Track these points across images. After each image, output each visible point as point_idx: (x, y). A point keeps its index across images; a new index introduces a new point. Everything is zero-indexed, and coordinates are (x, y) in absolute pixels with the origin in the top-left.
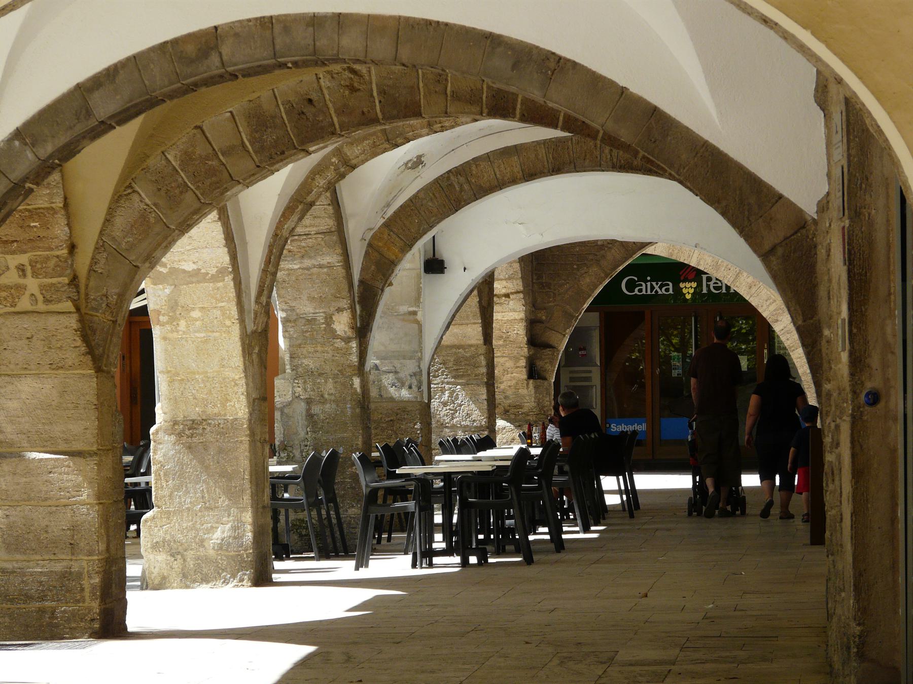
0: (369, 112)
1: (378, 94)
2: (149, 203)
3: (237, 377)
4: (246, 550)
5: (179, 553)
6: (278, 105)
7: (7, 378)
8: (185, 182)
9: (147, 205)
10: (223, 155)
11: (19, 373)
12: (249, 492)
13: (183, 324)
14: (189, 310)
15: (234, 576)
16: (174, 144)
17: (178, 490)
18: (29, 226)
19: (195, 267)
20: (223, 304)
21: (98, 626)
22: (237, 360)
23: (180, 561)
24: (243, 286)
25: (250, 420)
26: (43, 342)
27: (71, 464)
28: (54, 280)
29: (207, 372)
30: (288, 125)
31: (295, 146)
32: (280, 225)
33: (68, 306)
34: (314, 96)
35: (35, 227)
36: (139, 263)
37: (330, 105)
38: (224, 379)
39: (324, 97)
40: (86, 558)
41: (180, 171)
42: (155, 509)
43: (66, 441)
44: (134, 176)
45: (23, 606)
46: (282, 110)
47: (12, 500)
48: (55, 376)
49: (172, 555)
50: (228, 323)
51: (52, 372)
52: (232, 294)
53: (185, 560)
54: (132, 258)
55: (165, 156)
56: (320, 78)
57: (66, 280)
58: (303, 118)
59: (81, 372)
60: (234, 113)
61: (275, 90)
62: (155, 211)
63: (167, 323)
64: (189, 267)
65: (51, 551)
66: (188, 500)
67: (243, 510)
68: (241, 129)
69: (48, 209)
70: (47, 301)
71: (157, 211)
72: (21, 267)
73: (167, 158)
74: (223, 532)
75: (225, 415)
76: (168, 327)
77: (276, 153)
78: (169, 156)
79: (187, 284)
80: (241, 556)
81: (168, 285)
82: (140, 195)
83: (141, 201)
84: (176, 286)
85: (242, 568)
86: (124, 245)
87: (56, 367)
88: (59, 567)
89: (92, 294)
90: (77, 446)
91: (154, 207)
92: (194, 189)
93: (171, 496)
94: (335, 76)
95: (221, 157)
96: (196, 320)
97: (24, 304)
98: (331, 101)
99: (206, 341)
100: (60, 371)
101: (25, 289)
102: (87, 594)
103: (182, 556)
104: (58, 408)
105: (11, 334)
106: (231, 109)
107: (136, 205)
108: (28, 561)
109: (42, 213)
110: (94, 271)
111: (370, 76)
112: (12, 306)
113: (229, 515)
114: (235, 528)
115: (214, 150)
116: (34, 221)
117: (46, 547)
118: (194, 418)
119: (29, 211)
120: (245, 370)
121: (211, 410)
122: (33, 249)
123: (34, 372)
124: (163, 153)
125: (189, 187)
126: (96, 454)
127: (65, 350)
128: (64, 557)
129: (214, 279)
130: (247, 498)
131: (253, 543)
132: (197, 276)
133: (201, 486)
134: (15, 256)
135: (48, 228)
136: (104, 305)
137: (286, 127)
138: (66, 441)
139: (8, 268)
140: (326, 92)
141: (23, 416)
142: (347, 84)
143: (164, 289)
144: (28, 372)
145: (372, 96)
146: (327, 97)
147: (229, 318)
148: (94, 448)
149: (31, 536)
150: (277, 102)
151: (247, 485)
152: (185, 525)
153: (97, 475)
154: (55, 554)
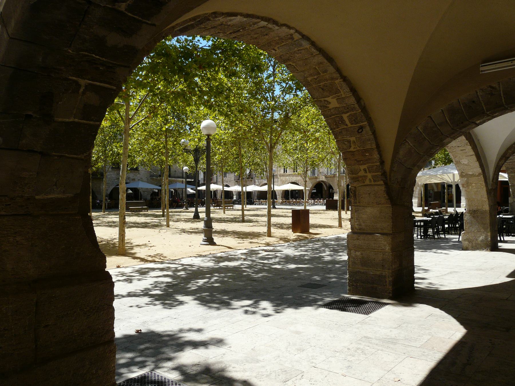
2: (412, 145)
7: (363, 207)
8: (425, 137)
9: (411, 146)
10: (439, 126)
12: (489, 228)
13: (470, 187)
15: (486, 249)
25: (490, 211)
27: (383, 238)
28: (376, 174)
32: (498, 163)
35: (368, 155)
40: (387, 271)
49: (469, 242)
50: (482, 187)
52: (483, 179)
57: (380, 174)
59: (387, 205)
61: (459, 99)
64: (471, 173)
67: (488, 232)
68: (446, 115)
69: (371, 148)
70: (375, 181)
73: (418, 129)
74: (482, 237)
76: (467, 188)
78: (419, 128)
82: (409, 143)
85: (488, 247)
87: (378, 204)
88: (378, 273)
90: (385, 231)
93: (469, 228)
94: (484, 90)
97: (367, 182)
98: (482, 101)
99: (477, 191)
106: (442, 109)
111: (499, 87)
112: (363, 183)
113: (484, 234)
114: (486, 237)
115: (435, 124)
118: (475, 209)
120: (488, 198)
123: (371, 205)
124: (417, 127)
126: (391, 234)
129: (478, 176)
130: (489, 230)
132: (473, 175)
134: (362, 166)
139: (361, 170)
140: (480, 97)
144: (369, 205)
146: (481, 99)
148: (391, 232)
150: (460, 103)
151: (489, 226)
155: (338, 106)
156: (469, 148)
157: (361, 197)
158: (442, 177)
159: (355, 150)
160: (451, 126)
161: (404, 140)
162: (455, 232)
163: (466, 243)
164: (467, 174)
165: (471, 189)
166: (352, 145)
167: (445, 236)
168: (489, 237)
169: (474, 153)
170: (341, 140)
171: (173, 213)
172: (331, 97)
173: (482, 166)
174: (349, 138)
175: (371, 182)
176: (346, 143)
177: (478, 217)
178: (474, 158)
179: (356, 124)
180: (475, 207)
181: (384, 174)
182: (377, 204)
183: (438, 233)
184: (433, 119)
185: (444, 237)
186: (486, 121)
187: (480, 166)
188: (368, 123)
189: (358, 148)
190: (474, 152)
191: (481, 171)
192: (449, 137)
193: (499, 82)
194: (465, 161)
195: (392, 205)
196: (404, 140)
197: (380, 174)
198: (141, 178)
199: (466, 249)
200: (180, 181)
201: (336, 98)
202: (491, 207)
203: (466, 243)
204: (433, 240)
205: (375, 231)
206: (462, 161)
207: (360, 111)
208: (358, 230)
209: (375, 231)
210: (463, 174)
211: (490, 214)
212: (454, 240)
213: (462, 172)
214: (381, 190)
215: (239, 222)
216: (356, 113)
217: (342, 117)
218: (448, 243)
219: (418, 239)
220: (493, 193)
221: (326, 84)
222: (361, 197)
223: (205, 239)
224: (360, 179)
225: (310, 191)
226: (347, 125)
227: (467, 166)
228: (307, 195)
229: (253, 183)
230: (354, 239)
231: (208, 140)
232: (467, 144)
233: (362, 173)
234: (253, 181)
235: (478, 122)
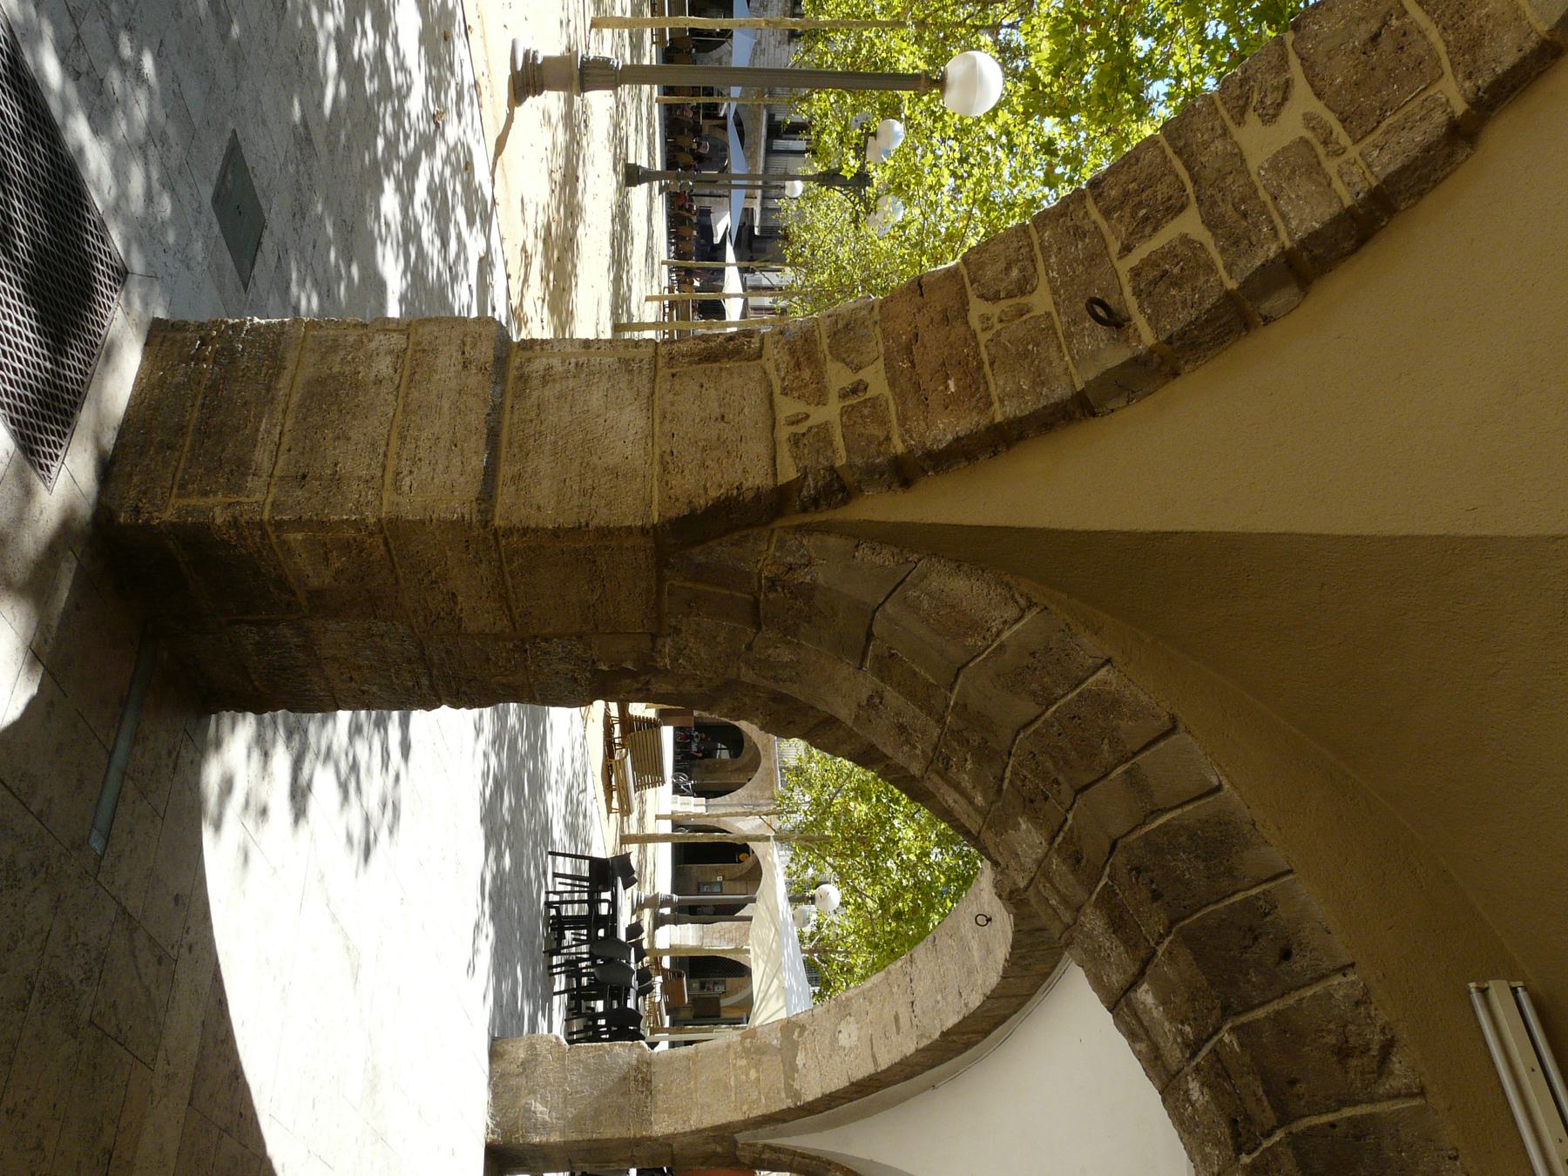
0: (1300, 1097)
1: (1349, 1118)
3: (692, 1122)
4: (522, 1136)
5: (524, 1069)
6: (1260, 884)
9: (999, 633)
10: (1126, 772)
11: (656, 409)
12: (580, 1138)
13: (744, 1062)
14: (756, 1067)
15: (497, 1125)
16: (1129, 680)
17: (585, 1068)
18: (947, 377)
19: (800, 1066)
20: (763, 1101)
21: (122, 520)
22: (708, 1121)
23: (517, 1071)
24: (781, 1126)
25: (650, 1138)
26: (715, 438)
29: (696, 1091)
30: (1221, 905)
31: (1178, 921)
33: (788, 473)
34: (1299, 963)
35: (947, 387)
36: (958, 264)
37: (1291, 1000)
38: (690, 1109)
39: (1304, 986)
40: (270, 500)
41: (1078, 691)
42: (568, 1046)
43: (517, 478)
44: (1053, 607)
45: (199, 402)
46: (1254, 892)
47: (409, 388)
48: (649, 461)
49: (522, 1063)
50: (745, 1108)
51: (657, 457)
52: (774, 1108)
53: (518, 1076)
54: (889, 608)
55: (1103, 665)
56: (1345, 975)
57: (841, 460)
58: (1244, 937)
59: (655, 502)
60: (1217, 795)
61: (1291, 877)
62: (988, 647)
63: (743, 1047)
64: (800, 1060)
65: (297, 444)
66: (574, 1078)
67: (563, 1133)
68: (1189, 807)
71: (989, 650)
72: (862, 387)
74: (541, 1113)
75: (655, 1112)
77: (1152, 882)
78: (1103, 672)
79: (782, 1061)
80: (517, 1132)
82: (1017, 621)
83: (1005, 622)
84: (780, 1049)
86: (912, 593)
88: (262, 457)
89: (812, 540)
91: (995, 645)
92: (1043, 718)
95: (1120, 770)
96: (747, 1075)
97: (788, 407)
98: (1301, 1000)
99: (726, 1087)
100: (657, 468)
101: (818, 404)
102: (194, 501)
103: (522, 1073)
104: (584, 465)
105: (730, 392)
106: (1226, 786)
107: (996, 614)
108: (285, 412)
109: (978, 388)
110: (857, 546)
111: (1397, 1096)
113: (557, 1118)
114: (545, 1124)
115: (1135, 754)
116: (958, 381)
117: (305, 437)
119: (980, 367)
120: (699, 1131)
121: (660, 1098)
122: (901, 398)
124: (1108, 661)
125: (1047, 709)
126: (485, 524)
127: (699, 473)
128: (280, 463)
130: (574, 1136)
131: (528, 1144)
132: (791, 1069)
133: (587, 1090)
135: (946, 408)
136: (790, 559)
137: (1217, 902)
138: (517, 478)
139: (858, 368)
140: (1318, 988)
141: (571, 413)
142: (1351, 1040)
143: (777, 1039)
144: (657, 421)
145: (1343, 1103)
146: (1309, 992)
147: (750, 1109)
148: (498, 522)
149: (334, 416)
150: (1266, 881)
151: (586, 1136)
152: (551, 1075)
153: (438, 520)
154: (289, 450)
155: (1253, 165)
156: (907, 1046)
157: (704, 380)
158: (771, 996)
159: (975, 322)
160: (1133, 836)
161: (1029, 600)
162: (577, 1033)
163: (521, 1051)
164: (794, 1046)
165: (734, 1065)
166: (1004, 305)
167: (560, 993)
168: (544, 1139)
169: (883, 1066)
170: (1031, 245)
171: (648, 131)
172: (1317, 107)
173: (830, 1101)
174: (1043, 279)
175: (793, 423)
176: (1015, 273)
177: (624, 1094)
178: (864, 1070)
179: (1137, 293)
180: (665, 1084)
181: (838, 489)
182: (662, 456)
183: (572, 969)
184: (1162, 744)
185: (556, 989)
186: (1142, 1046)
187: (831, 1093)
188: (1151, 351)
189: (983, 338)
190: (889, 1069)
191: (810, 1099)
192: (1051, 841)
193: (1422, 1093)
194: (849, 1034)
195: (654, 526)
196: (1029, 600)
197: (838, 464)
198: (763, 52)
199: (494, 1054)
201: (1308, 135)
202: (668, 1141)
203: (521, 1051)
204: (540, 943)
205: (510, 444)
207: (1232, 285)
208: (521, 366)
209: (510, 444)
211: (635, 1138)
212: (543, 1024)
213: (803, 1028)
214: (745, 471)
215: (615, 313)
216: (1210, 268)
217: (1182, 208)
218: (529, 995)
219: (548, 893)
220: (719, 1149)
221: (1415, 36)
222: (704, 380)
223: (535, 58)
224: (806, 374)
226: (1127, 249)
227: (831, 1044)
230: (467, 348)
231: (923, 81)
232: (921, 1036)
233: (838, 376)
235: (1145, 996)
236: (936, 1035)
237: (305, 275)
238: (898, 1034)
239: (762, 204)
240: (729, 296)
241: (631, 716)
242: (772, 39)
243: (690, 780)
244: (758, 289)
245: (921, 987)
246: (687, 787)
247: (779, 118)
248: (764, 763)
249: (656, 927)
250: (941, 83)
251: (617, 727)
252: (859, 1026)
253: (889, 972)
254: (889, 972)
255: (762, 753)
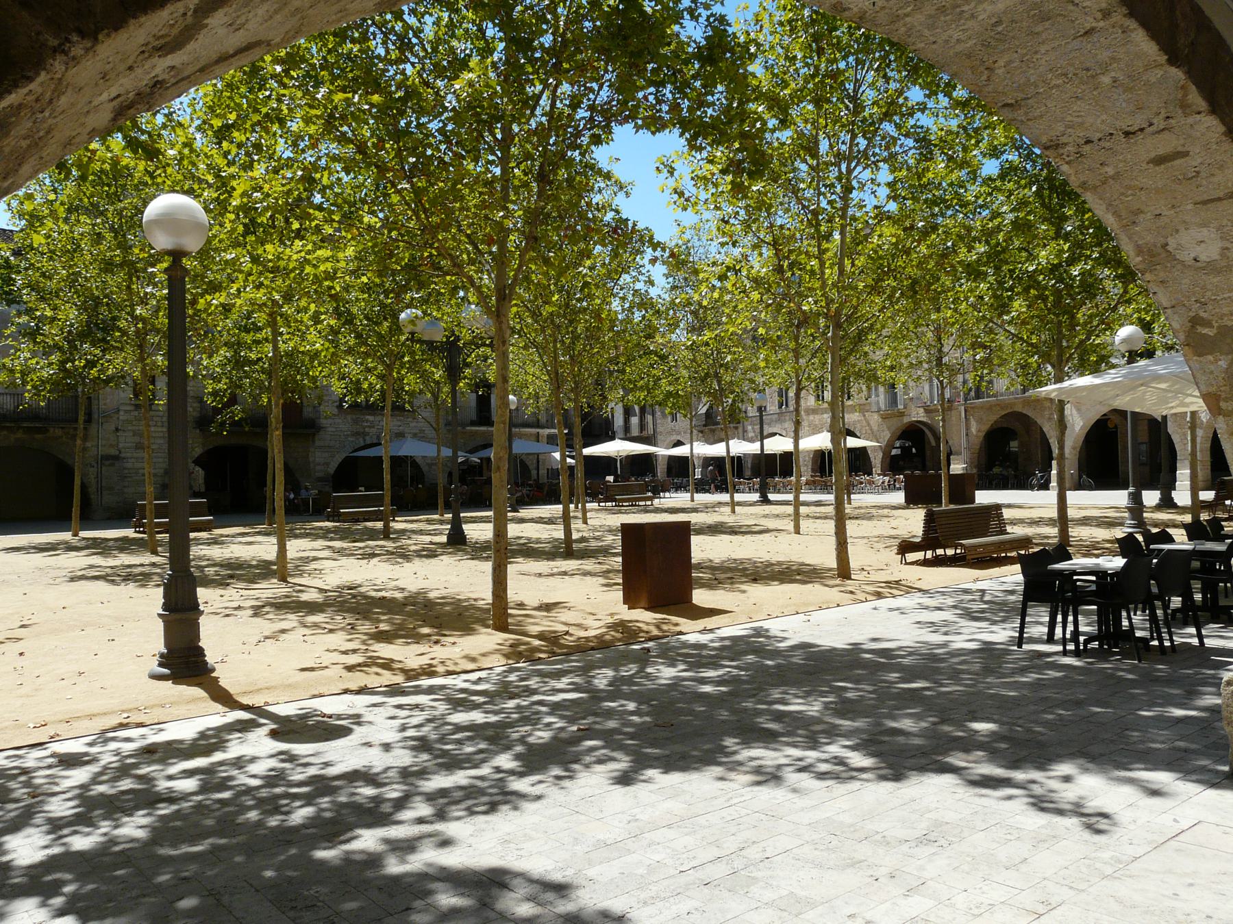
81: (1221, 355)
143: (1217, 361)
167: (1200, 637)
185: (1195, 641)
200: (531, 435)
206: (1180, 247)
210: (1205, 331)
213: (1196, 321)
218: (1189, 695)
225: (886, 451)
228: (876, 460)
229: (741, 435)
232: (1184, 106)
234: (740, 430)
236: (1177, 74)
237: (831, 687)
238: (1186, 154)
239: (543, 427)
240: (728, 451)
241: (923, 539)
242: (412, 425)
243: (1035, 474)
244: (627, 428)
245: (1098, 122)
246: (1042, 477)
247: (474, 418)
248: (1019, 408)
249: (1174, 506)
250: (177, 255)
251: (940, 552)
252: (1182, 228)
253: (1083, 185)
254: (1083, 185)
255: (1009, 411)
